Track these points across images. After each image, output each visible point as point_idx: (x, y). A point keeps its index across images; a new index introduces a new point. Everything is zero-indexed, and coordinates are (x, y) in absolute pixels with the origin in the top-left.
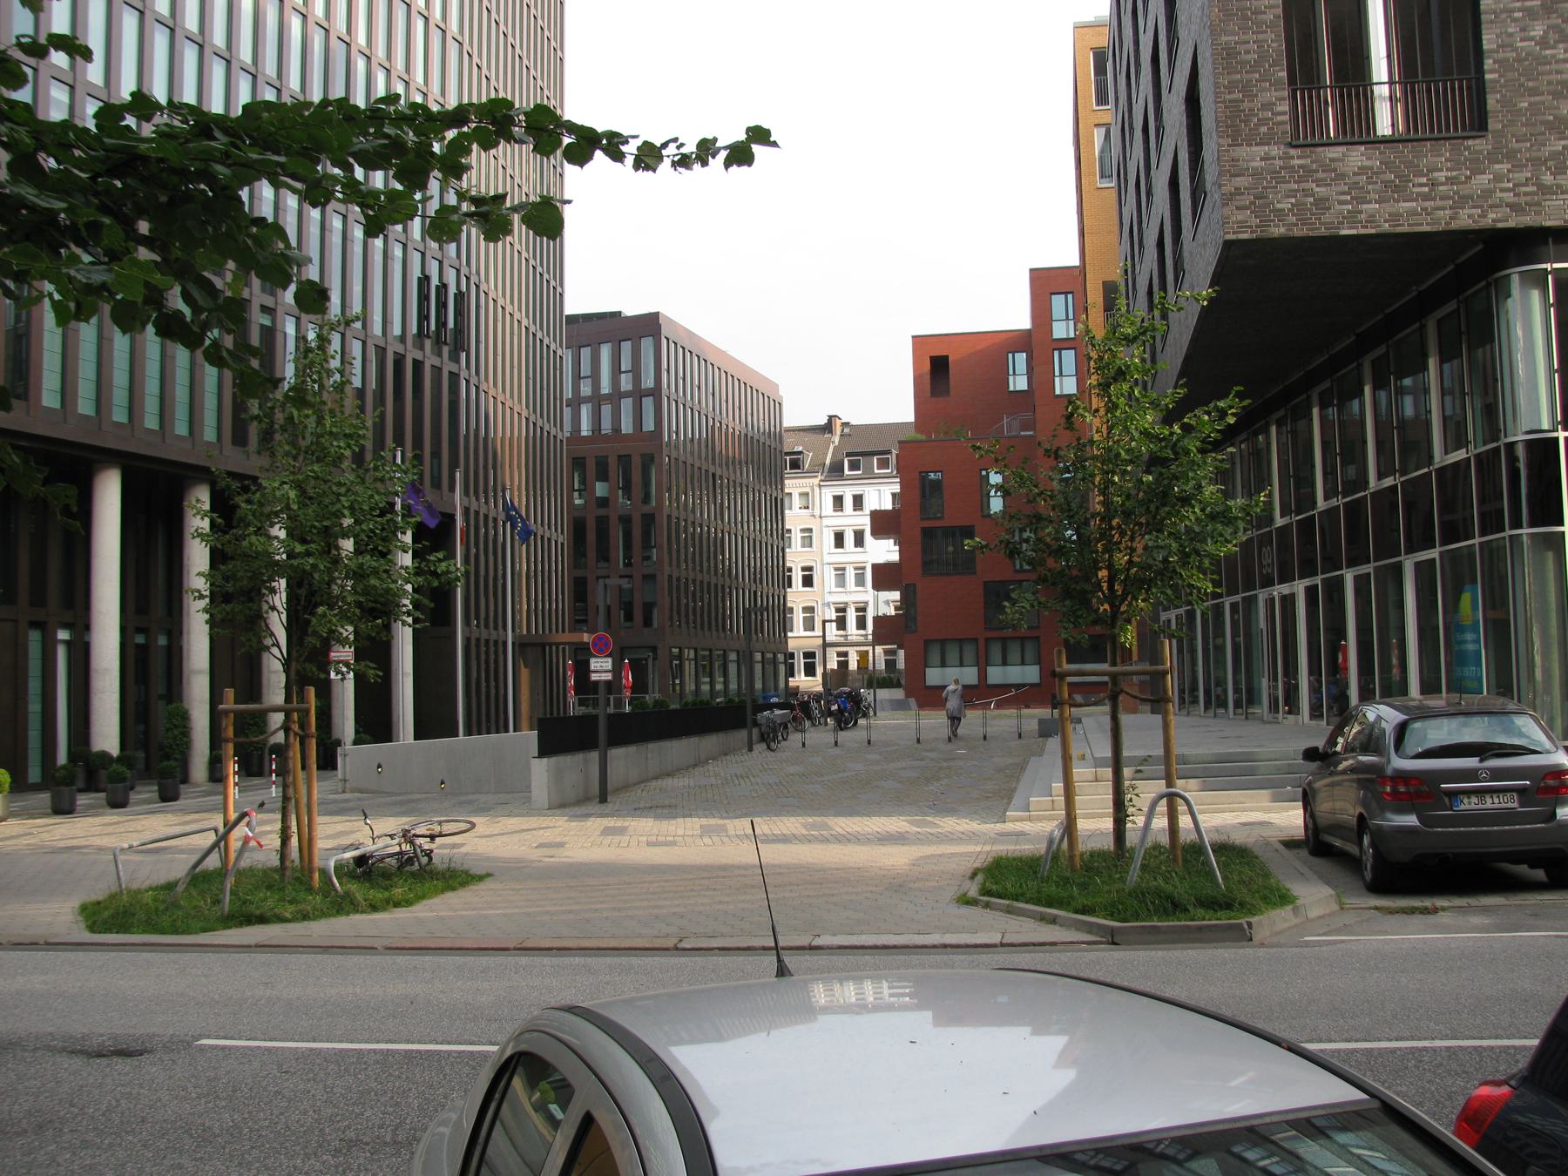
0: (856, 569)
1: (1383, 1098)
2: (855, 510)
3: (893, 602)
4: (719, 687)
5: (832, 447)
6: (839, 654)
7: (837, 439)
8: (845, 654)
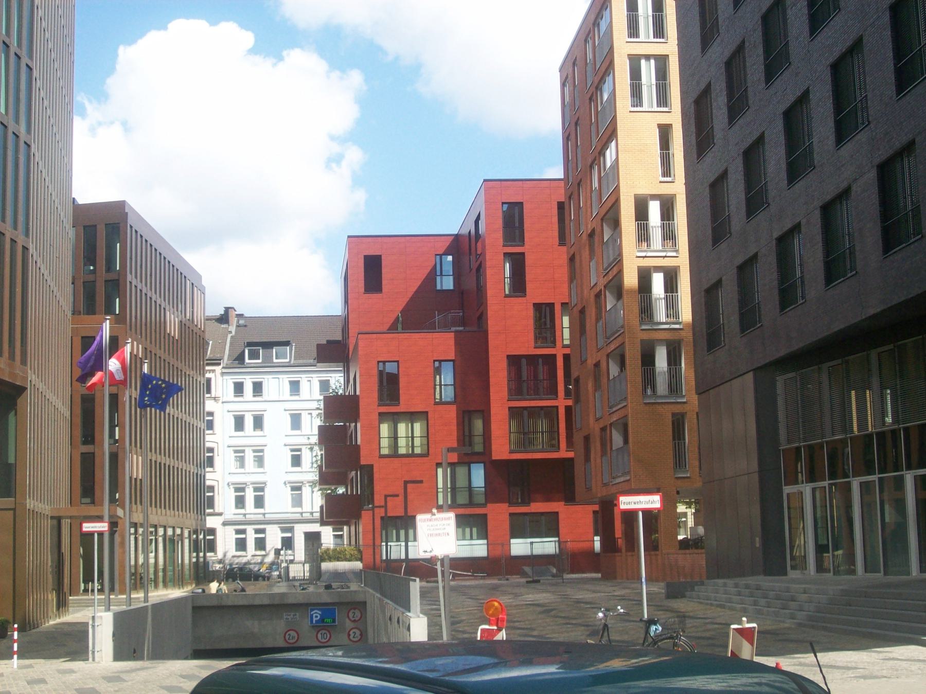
0: (254, 451)
1: (565, 142)
2: (254, 396)
3: (290, 483)
4: (201, 554)
5: (229, 336)
6: (257, 531)
7: (233, 328)
8: (243, 532)
